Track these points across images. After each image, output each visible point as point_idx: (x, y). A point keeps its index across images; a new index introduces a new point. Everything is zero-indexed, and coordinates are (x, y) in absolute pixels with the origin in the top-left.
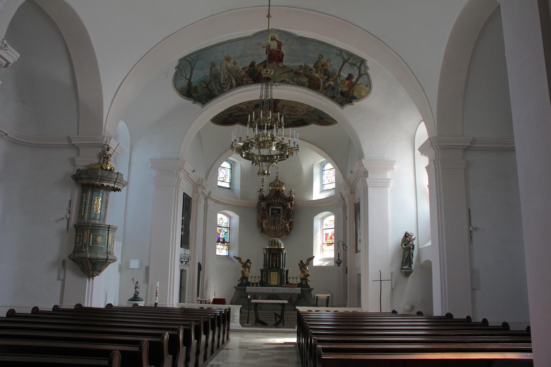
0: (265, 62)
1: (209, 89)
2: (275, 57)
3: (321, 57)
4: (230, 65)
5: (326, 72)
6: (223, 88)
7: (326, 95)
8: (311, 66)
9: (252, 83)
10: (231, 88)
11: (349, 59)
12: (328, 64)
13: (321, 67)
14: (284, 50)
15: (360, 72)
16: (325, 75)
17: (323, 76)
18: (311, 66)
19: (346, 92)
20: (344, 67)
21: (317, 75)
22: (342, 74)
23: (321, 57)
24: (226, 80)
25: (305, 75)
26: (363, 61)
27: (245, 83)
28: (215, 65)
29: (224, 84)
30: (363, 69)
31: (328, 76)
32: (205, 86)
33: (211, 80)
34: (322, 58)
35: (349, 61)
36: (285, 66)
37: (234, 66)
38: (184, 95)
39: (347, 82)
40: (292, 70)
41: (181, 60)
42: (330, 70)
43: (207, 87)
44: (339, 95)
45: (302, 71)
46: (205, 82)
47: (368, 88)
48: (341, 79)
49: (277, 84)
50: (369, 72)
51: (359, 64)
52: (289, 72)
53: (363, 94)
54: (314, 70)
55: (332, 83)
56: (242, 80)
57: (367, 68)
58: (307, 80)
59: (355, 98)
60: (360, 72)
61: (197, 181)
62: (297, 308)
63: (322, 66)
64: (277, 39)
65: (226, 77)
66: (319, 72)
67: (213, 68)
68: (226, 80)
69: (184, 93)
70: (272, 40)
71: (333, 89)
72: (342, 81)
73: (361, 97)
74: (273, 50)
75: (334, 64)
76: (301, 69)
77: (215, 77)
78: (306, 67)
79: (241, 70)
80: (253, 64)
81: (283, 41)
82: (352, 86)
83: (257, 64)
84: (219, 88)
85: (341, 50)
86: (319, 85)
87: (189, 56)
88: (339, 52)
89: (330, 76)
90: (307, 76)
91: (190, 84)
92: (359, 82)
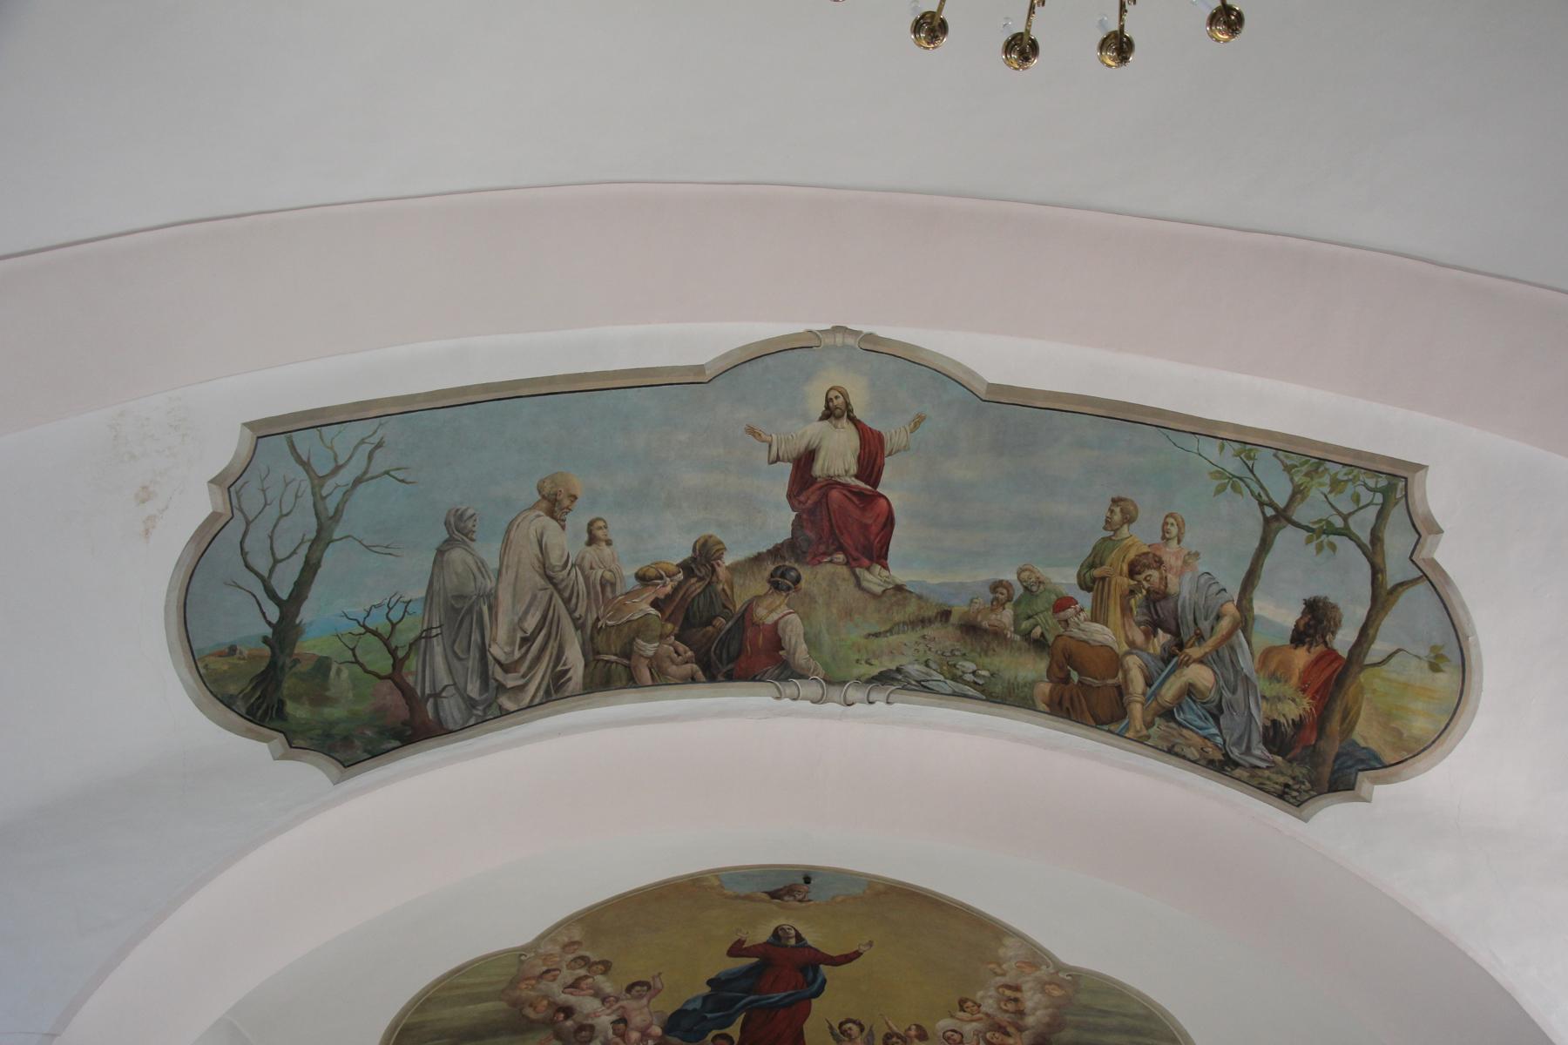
0: (791, 548)
1: (406, 691)
2: (841, 517)
3: (1123, 511)
4: (566, 542)
5: (1158, 612)
6: (501, 688)
7: (1172, 752)
8: (1064, 578)
9: (693, 679)
10: (556, 690)
11: (1298, 493)
12: (1171, 555)
13: (1127, 582)
14: (894, 486)
15: (1377, 571)
16: (1154, 625)
17: (1139, 637)
18: (1064, 578)
19: (1298, 725)
20: (1269, 561)
21: (1102, 634)
22: (1262, 606)
23: (1123, 511)
24: (527, 641)
25: (1026, 635)
26: (1393, 483)
27: (645, 674)
28: (468, 534)
30: (1396, 543)
31: (1176, 633)
32: (384, 664)
33: (426, 635)
34: (1129, 519)
35: (1302, 513)
36: (899, 588)
37: (591, 553)
38: (228, 702)
39: (1302, 658)
40: (945, 615)
41: (263, 432)
42: (1183, 587)
43: (396, 676)
44: (1259, 750)
45: (1006, 616)
47: (1445, 680)
48: (1261, 640)
49: (853, 694)
50: (1446, 554)
51: (1370, 514)
52: (924, 622)
53: (1420, 725)
54: (1085, 600)
55: (1201, 676)
56: (627, 653)
57: (1423, 529)
58: (1042, 665)
59: (1372, 762)
60: (1377, 571)
62: (755, 960)
63: (1133, 571)
64: (858, 414)
65: (531, 624)
66: (1115, 614)
67: (456, 555)
68: (527, 641)
69: (233, 689)
70: (829, 414)
71: (1216, 714)
72: (1268, 653)
73: (1411, 751)
74: (832, 483)
75: (1208, 548)
76: (997, 604)
77: (461, 612)
78: (1032, 589)
79: (632, 583)
80: (705, 556)
81: (892, 429)
82: (1333, 680)
83: (728, 560)
84: (473, 689)
85: (1247, 444)
86: (1121, 691)
87: (320, 421)
88: (1233, 465)
89: (1187, 634)
90: (1040, 644)
91: (284, 633)
92: (1379, 649)
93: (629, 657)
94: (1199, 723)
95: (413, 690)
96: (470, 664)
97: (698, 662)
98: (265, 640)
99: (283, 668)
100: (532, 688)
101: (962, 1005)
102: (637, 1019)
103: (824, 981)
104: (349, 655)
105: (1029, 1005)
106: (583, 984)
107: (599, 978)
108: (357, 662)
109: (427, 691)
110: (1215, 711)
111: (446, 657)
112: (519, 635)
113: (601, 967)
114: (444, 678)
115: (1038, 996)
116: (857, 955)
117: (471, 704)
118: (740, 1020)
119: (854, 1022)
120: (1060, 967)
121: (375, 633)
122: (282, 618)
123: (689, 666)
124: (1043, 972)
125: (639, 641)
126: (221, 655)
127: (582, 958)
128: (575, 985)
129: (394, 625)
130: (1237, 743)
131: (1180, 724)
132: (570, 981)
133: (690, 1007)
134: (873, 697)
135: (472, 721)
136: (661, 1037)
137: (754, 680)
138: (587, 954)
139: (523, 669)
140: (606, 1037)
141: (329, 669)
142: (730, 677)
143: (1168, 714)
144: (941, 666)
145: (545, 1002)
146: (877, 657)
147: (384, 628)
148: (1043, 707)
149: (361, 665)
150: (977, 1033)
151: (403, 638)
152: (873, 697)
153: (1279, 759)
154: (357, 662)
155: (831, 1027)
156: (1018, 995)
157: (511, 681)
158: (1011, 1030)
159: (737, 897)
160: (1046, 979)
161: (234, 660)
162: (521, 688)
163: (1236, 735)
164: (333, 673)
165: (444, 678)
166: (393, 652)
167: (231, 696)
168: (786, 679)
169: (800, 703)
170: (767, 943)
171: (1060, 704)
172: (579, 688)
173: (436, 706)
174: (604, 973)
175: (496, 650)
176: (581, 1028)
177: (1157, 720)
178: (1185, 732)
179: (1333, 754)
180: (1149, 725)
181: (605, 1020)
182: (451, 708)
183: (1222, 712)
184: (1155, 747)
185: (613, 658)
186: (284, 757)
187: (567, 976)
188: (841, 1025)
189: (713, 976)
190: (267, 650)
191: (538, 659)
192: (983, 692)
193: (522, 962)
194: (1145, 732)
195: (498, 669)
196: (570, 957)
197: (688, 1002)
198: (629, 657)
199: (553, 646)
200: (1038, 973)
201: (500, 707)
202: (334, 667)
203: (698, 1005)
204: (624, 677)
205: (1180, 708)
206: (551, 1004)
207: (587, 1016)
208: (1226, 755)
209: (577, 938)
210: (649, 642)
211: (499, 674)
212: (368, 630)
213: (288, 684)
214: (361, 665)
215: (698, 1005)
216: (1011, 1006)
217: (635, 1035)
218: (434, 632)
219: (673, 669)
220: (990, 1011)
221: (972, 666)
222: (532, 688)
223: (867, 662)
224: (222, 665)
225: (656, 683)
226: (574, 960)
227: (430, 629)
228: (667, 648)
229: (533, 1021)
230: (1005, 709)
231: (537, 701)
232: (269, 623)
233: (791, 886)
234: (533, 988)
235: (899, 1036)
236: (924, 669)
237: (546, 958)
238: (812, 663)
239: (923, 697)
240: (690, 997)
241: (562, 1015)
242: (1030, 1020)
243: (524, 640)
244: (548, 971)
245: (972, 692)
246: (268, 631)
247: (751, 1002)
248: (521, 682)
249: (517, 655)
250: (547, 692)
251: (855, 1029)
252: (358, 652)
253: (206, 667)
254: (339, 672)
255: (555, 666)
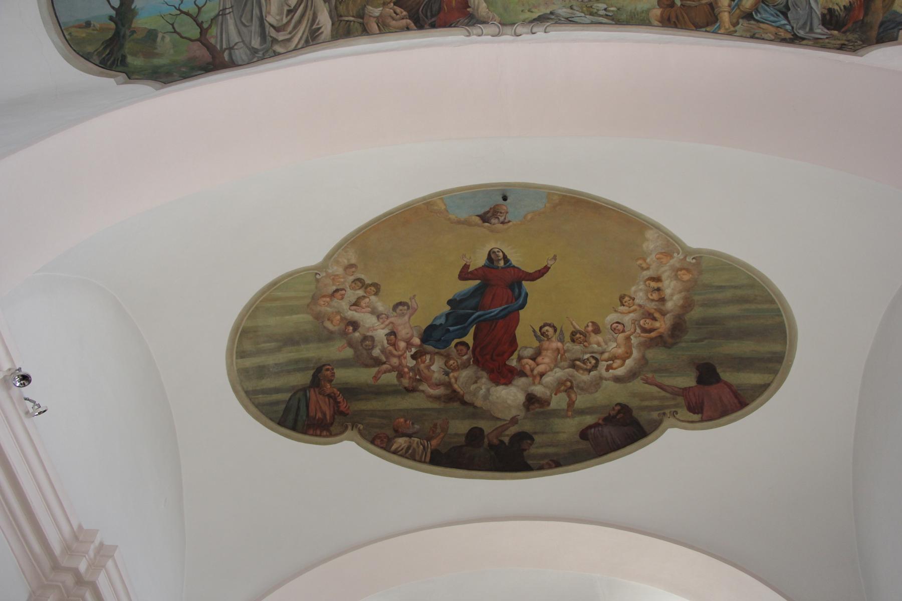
1: (209, 47)
6: (275, 41)
9: (408, 29)
10: (313, 39)
29: (278, 29)
32: (195, 32)
33: (222, 13)
38: (87, 57)
43: (202, 39)
44: (819, 30)
46: (195, 19)
49: (520, 30)
56: (361, 15)
61: (68, 549)
62: (478, 282)
69: (90, 49)
84: (256, 43)
93: (362, 18)
94: (772, 18)
95: (215, 47)
96: (253, 28)
97: (410, 18)
98: (111, 18)
99: (124, 37)
100: (296, 40)
101: (622, 298)
102: (403, 332)
103: (527, 295)
104: (170, 28)
105: (668, 292)
106: (363, 303)
107: (373, 298)
108: (175, 32)
109: (224, 47)
110: (784, 10)
111: (236, 25)
112: (286, 8)
113: (373, 288)
114: (235, 38)
115: (673, 283)
116: (546, 269)
117: (254, 51)
118: (472, 330)
119: (549, 325)
120: (688, 252)
121: (187, 14)
122: (122, 4)
123: (404, 21)
124: (675, 261)
125: (370, 8)
126: (80, 27)
127: (359, 280)
128: (356, 304)
129: (199, 9)
130: (803, 27)
131: (758, 21)
132: (353, 300)
133: (438, 322)
134: (534, 30)
135: (255, 59)
136: (420, 346)
137: (450, 26)
138: (362, 276)
139: (290, 28)
140: (383, 346)
141: (157, 37)
142: (433, 26)
143: (749, 16)
144: (582, 8)
145: (338, 317)
146: (535, 7)
147: (193, 10)
148: (656, 23)
149: (179, 34)
150: (634, 321)
151: (206, 17)
152: (534, 30)
153: (836, 32)
154: (175, 32)
155: (534, 331)
156: (659, 285)
157: (281, 36)
158: (657, 315)
159: (459, 222)
160: (678, 265)
161: (89, 31)
162: (289, 40)
163: (801, 22)
164: (159, 39)
165: (235, 38)
166: (200, 25)
167: (89, 53)
168: (473, 25)
169: (483, 37)
170: (484, 266)
171: (669, 20)
172: (329, 37)
173: (230, 55)
174: (376, 294)
175: (270, 19)
176: (365, 338)
177: (741, 20)
178: (762, 25)
179: (879, 22)
180: (735, 24)
181: (381, 334)
182: (240, 53)
183: (789, 9)
184: (741, 36)
185: (352, 19)
186: (125, 83)
187: (352, 295)
188: (541, 328)
189: (451, 297)
190: (113, 25)
191: (299, 22)
192: (613, 20)
193: (318, 281)
194: (732, 29)
195: (272, 29)
196: (352, 278)
197: (436, 319)
198: (362, 18)
199: (309, 14)
200: (672, 262)
201: (274, 52)
202: (160, 35)
203: (442, 321)
204: (360, 29)
205: (757, 11)
206: (343, 319)
207: (369, 329)
208: (795, 35)
209: (353, 261)
210: (376, 7)
211: (273, 33)
212: (182, 12)
213: (128, 46)
214: (179, 34)
215: (442, 321)
216: (655, 296)
217: (402, 345)
218: (227, 11)
219: (393, 23)
220: (641, 302)
221: (603, 6)
222: (296, 40)
223: (530, 11)
224: (82, 33)
225: (381, 32)
226: (354, 281)
227: (225, 9)
228: (389, 11)
229: (332, 332)
230: (629, 28)
231: (300, 46)
232: (113, 8)
233: (494, 207)
234: (329, 305)
235: (581, 333)
236: (569, 11)
237: (334, 277)
238: (491, 15)
239: (570, 27)
240: (438, 314)
241: (351, 328)
242: (669, 305)
243: (289, 12)
244: (337, 291)
245: (604, 20)
246: (113, 13)
247: (479, 316)
248: (289, 36)
249: (285, 21)
250: (307, 42)
251: (551, 330)
252: (175, 25)
253: (70, 34)
254: (163, 38)
255: (312, 25)
